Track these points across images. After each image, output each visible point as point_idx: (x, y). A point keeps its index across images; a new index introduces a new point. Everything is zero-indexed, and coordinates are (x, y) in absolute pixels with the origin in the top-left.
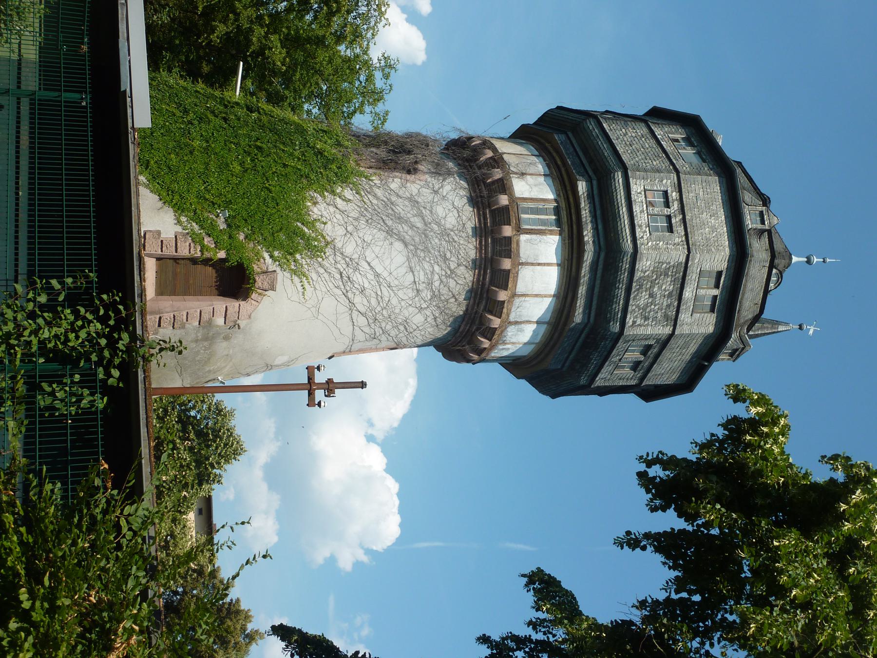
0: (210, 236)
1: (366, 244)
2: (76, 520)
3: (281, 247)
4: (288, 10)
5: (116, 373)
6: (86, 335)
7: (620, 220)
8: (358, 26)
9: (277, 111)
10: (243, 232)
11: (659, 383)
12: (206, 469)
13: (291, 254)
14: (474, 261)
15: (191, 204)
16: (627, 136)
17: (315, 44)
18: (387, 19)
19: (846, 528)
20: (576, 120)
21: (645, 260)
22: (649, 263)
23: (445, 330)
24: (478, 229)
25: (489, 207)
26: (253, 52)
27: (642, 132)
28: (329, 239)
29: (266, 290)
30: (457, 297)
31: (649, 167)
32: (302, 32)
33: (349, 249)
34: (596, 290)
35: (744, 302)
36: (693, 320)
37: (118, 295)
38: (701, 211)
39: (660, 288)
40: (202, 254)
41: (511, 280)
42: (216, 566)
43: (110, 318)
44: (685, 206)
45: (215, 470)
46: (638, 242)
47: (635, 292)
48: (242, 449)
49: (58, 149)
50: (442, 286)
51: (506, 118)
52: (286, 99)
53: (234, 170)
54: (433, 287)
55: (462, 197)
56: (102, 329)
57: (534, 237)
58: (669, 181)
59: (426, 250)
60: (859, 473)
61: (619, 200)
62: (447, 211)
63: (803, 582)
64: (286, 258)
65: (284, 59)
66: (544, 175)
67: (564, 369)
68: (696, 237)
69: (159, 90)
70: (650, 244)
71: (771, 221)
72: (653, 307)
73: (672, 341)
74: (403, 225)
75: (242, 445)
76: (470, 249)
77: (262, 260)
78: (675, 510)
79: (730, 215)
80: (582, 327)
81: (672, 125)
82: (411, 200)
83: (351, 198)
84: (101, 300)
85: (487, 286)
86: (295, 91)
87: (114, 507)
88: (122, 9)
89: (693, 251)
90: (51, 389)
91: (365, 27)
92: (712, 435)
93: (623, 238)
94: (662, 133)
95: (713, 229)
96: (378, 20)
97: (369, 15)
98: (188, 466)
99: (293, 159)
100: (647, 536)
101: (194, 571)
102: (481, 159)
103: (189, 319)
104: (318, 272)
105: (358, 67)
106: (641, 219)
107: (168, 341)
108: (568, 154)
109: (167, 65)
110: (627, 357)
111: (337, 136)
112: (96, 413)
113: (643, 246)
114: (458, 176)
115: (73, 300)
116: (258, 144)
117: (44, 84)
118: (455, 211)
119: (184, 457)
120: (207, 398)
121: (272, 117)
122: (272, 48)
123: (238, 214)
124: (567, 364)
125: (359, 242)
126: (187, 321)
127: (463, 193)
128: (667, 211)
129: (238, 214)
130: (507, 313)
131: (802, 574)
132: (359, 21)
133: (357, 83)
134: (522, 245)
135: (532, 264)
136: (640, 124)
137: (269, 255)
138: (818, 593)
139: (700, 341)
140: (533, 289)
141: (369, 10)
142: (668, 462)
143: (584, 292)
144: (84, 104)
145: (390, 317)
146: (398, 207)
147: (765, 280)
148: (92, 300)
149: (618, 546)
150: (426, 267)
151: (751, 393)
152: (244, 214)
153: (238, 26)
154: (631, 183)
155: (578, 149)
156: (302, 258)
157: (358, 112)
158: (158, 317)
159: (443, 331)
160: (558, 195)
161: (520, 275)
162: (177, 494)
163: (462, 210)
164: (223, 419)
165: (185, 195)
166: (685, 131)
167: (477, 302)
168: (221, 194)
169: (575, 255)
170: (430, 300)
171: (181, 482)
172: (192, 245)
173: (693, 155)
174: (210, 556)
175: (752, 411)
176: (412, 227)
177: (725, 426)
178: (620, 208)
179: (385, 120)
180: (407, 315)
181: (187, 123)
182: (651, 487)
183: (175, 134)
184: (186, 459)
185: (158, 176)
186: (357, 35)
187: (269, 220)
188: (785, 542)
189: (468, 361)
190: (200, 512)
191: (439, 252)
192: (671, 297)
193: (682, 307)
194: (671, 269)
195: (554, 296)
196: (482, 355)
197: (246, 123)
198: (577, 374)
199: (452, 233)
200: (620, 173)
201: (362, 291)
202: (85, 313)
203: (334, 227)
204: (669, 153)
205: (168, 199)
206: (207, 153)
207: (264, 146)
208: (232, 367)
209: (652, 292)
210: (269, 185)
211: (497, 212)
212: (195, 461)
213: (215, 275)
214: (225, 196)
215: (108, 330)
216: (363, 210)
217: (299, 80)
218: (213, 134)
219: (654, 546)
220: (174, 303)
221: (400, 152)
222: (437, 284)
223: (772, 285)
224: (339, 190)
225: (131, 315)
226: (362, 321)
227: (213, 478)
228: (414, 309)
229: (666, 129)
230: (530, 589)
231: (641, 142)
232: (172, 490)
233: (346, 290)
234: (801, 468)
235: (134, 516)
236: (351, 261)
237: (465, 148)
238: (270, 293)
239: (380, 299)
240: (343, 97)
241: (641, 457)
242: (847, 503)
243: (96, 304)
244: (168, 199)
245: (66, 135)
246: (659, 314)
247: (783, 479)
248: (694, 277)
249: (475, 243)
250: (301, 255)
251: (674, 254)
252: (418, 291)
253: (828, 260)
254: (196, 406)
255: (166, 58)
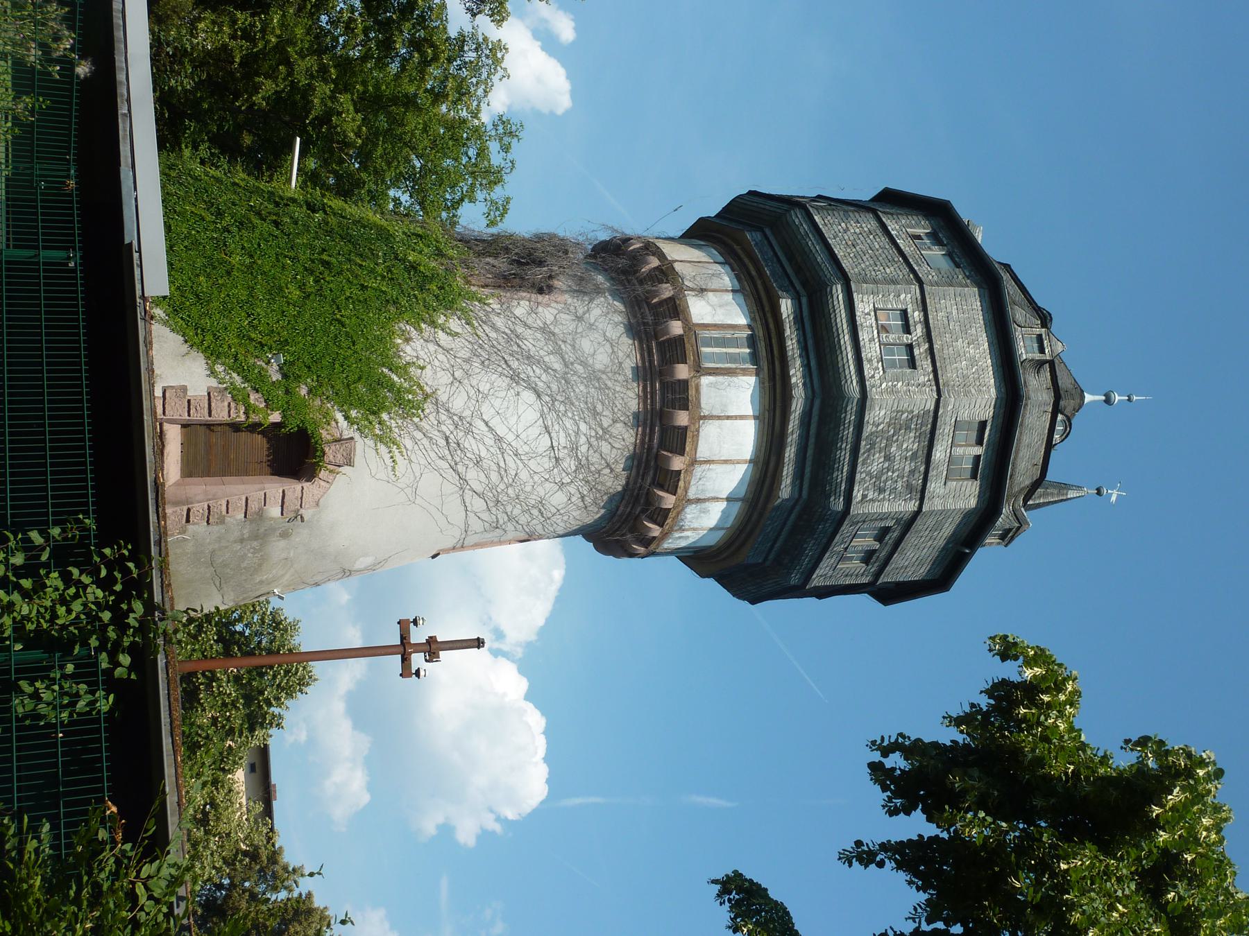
0: (257, 392)
1: (481, 396)
2: (72, 893)
3: (361, 403)
4: (365, 58)
5: (125, 659)
6: (82, 608)
7: (841, 353)
8: (464, 79)
9: (352, 210)
10: (306, 384)
11: (901, 580)
12: (260, 707)
13: (374, 413)
14: (636, 415)
15: (230, 347)
16: (849, 233)
17: (404, 105)
18: (505, 69)
19: (1161, 839)
20: (775, 212)
21: (877, 409)
22: (883, 413)
23: (597, 513)
24: (640, 369)
25: (656, 338)
26: (316, 118)
27: (869, 226)
28: (428, 390)
29: (339, 466)
30: (613, 466)
31: (880, 276)
32: (384, 87)
33: (459, 403)
34: (810, 452)
35: (1019, 461)
36: (947, 491)
37: (126, 547)
38: (954, 337)
39: (900, 447)
40: (248, 417)
41: (689, 440)
42: (277, 846)
43: (115, 581)
44: (932, 330)
45: (272, 709)
46: (867, 383)
47: (864, 453)
48: (310, 677)
49: (33, 270)
50: (591, 452)
51: (676, 210)
52: (364, 185)
53: (290, 296)
54: (579, 454)
55: (617, 324)
56: (105, 597)
57: (720, 379)
58: (909, 295)
59: (568, 401)
60: (1177, 763)
61: (839, 325)
62: (596, 345)
63: (1103, 918)
64: (368, 419)
65: (359, 127)
66: (732, 291)
67: (768, 563)
68: (949, 375)
69: (181, 184)
70: (884, 385)
71: (1054, 347)
72: (890, 474)
73: (919, 521)
74: (534, 367)
75: (311, 671)
76: (630, 399)
77: (333, 423)
78: (923, 811)
79: (995, 341)
80: (792, 504)
81: (912, 215)
82: (545, 330)
83: (459, 330)
84: (103, 556)
85: (655, 450)
86: (376, 172)
87: (127, 868)
88: (124, 123)
89: (945, 395)
90: (32, 689)
91: (474, 80)
92: (973, 705)
93: (845, 378)
94: (897, 227)
95: (973, 362)
96: (492, 70)
97: (480, 64)
98: (234, 704)
99: (375, 278)
100: (885, 847)
101: (245, 853)
102: (643, 270)
103: (230, 510)
104: (413, 438)
105: (465, 135)
106: (871, 350)
107: (199, 609)
108: (765, 260)
109: (191, 139)
110: (856, 544)
111: (437, 242)
112: (97, 721)
113: (874, 389)
114: (611, 295)
115: (63, 556)
116: (325, 257)
117: (15, 240)
118: (608, 345)
119: (228, 692)
120: (259, 605)
121: (343, 217)
122: (341, 113)
123: (298, 359)
124: (771, 557)
125: (472, 392)
126: (227, 513)
127: (618, 318)
128: (907, 338)
129: (298, 359)
130: (685, 487)
131: (1101, 907)
132: (464, 73)
133: (464, 160)
134: (704, 391)
135: (719, 418)
136: (867, 215)
137: (343, 416)
138: (1125, 932)
139: (957, 520)
140: (720, 452)
141: (479, 57)
142: (913, 749)
143: (792, 455)
144: (72, 264)
145: (518, 497)
146: (525, 342)
147: (1047, 431)
148: (89, 555)
149: (844, 863)
150: (568, 425)
151: (1024, 648)
152: (306, 358)
153: (292, 82)
154: (856, 300)
155: (780, 253)
156: (390, 418)
157: (466, 200)
158: (185, 508)
159: (595, 514)
160: (753, 319)
161: (702, 434)
162: (219, 746)
163: (617, 343)
164: (282, 635)
165: (222, 334)
166: (930, 223)
167: (641, 473)
168: (273, 331)
169: (778, 404)
170: (575, 471)
171: (223, 727)
172: (233, 405)
173: (942, 258)
174: (268, 833)
175: (1026, 675)
176: (547, 369)
177: (990, 693)
178: (841, 336)
179: (505, 210)
180: (542, 494)
181: (222, 230)
182: (888, 783)
183: (204, 247)
184: (230, 694)
185: (181, 309)
186: (462, 92)
187: (342, 366)
188: (1077, 863)
189: (632, 555)
190: (252, 768)
191: (586, 403)
192: (916, 459)
193: (932, 473)
194: (915, 420)
195: (751, 461)
196: (650, 547)
197: (307, 228)
198: (786, 571)
199: (604, 376)
200: (839, 287)
201: (478, 462)
202: (80, 575)
203: (435, 373)
204: (907, 255)
205: (197, 340)
206: (252, 273)
207: (333, 260)
208: (293, 575)
209: (888, 453)
210: (341, 316)
211: (667, 345)
212: (245, 697)
213: (266, 446)
214: (279, 334)
215: (112, 598)
216: (476, 347)
217: (381, 157)
218: (259, 245)
219: (896, 861)
220: (209, 488)
221: (527, 264)
222: (584, 449)
223: (1056, 437)
224: (441, 319)
225: (145, 575)
226: (478, 504)
227: (270, 720)
228: (552, 484)
229: (903, 221)
230: (724, 901)
231: (869, 241)
232: (212, 739)
233: (455, 461)
234: (1098, 749)
235: (156, 878)
236: (461, 420)
237: (620, 254)
238: (345, 469)
239: (503, 473)
240: (446, 180)
241: (874, 743)
242: (1162, 806)
243: (96, 562)
244: (197, 340)
245: (44, 241)
246: (899, 484)
247: (1072, 767)
248: (946, 431)
249: (637, 390)
250: (389, 413)
251: (918, 397)
252: (557, 459)
253: (1135, 398)
254: (243, 617)
255: (190, 130)
